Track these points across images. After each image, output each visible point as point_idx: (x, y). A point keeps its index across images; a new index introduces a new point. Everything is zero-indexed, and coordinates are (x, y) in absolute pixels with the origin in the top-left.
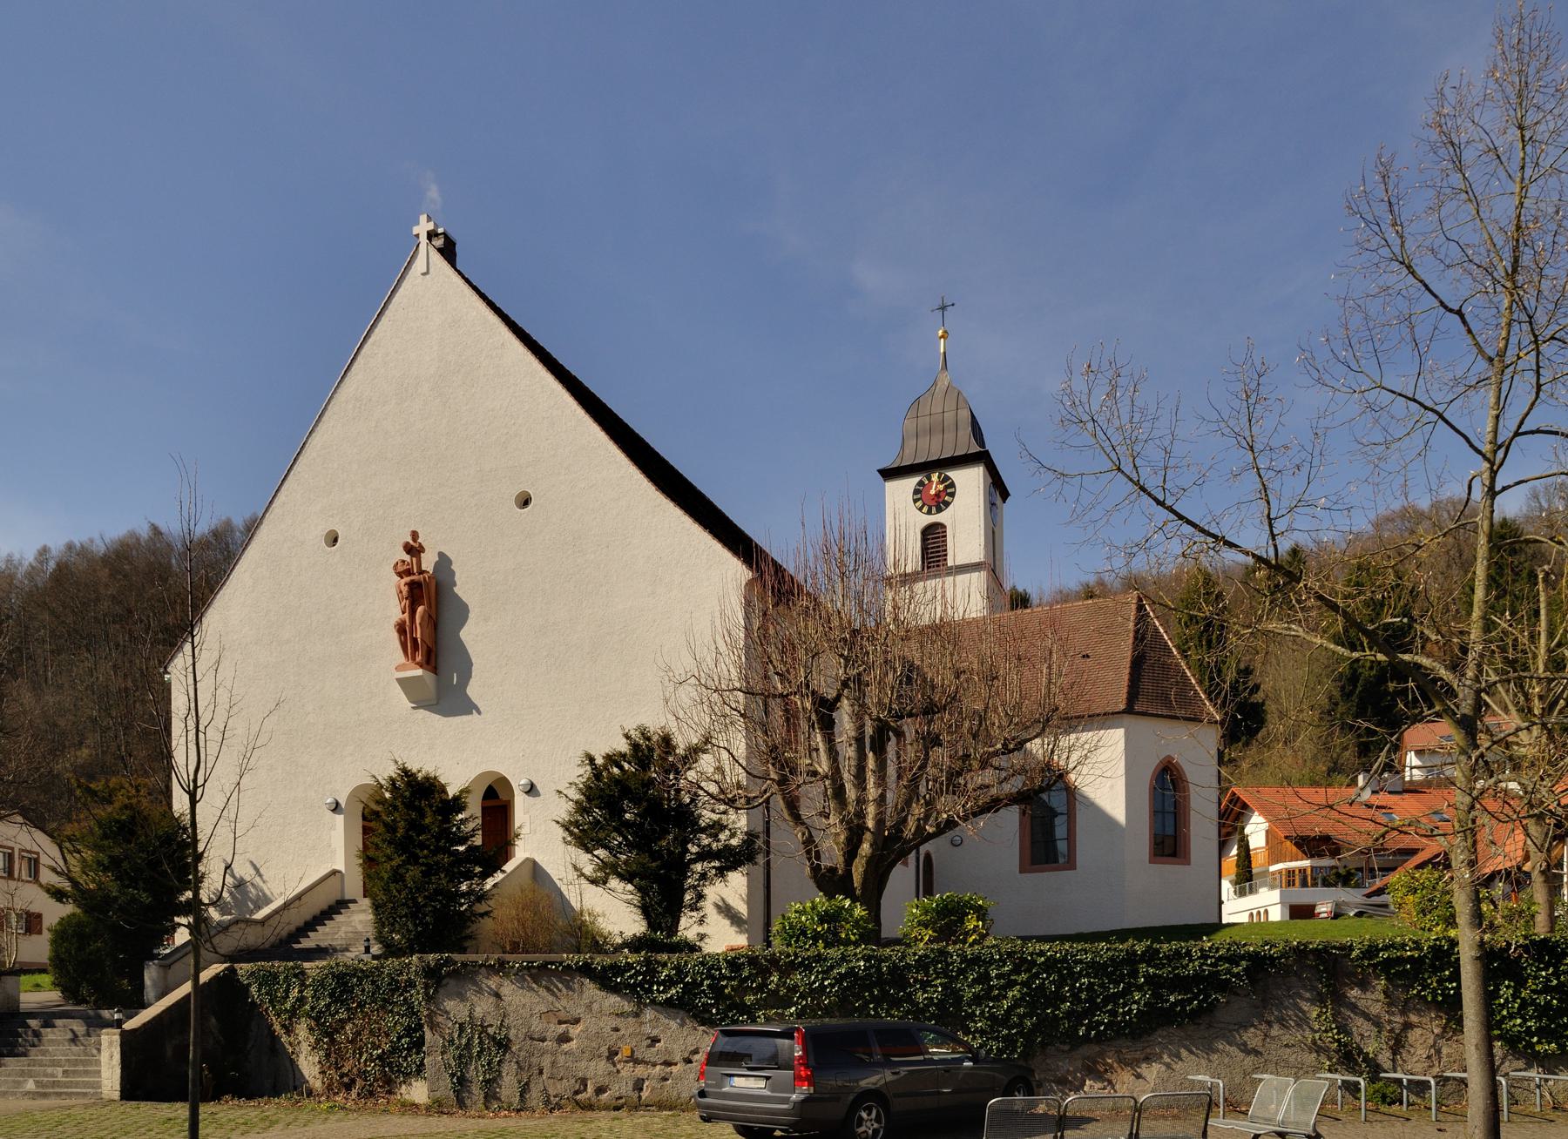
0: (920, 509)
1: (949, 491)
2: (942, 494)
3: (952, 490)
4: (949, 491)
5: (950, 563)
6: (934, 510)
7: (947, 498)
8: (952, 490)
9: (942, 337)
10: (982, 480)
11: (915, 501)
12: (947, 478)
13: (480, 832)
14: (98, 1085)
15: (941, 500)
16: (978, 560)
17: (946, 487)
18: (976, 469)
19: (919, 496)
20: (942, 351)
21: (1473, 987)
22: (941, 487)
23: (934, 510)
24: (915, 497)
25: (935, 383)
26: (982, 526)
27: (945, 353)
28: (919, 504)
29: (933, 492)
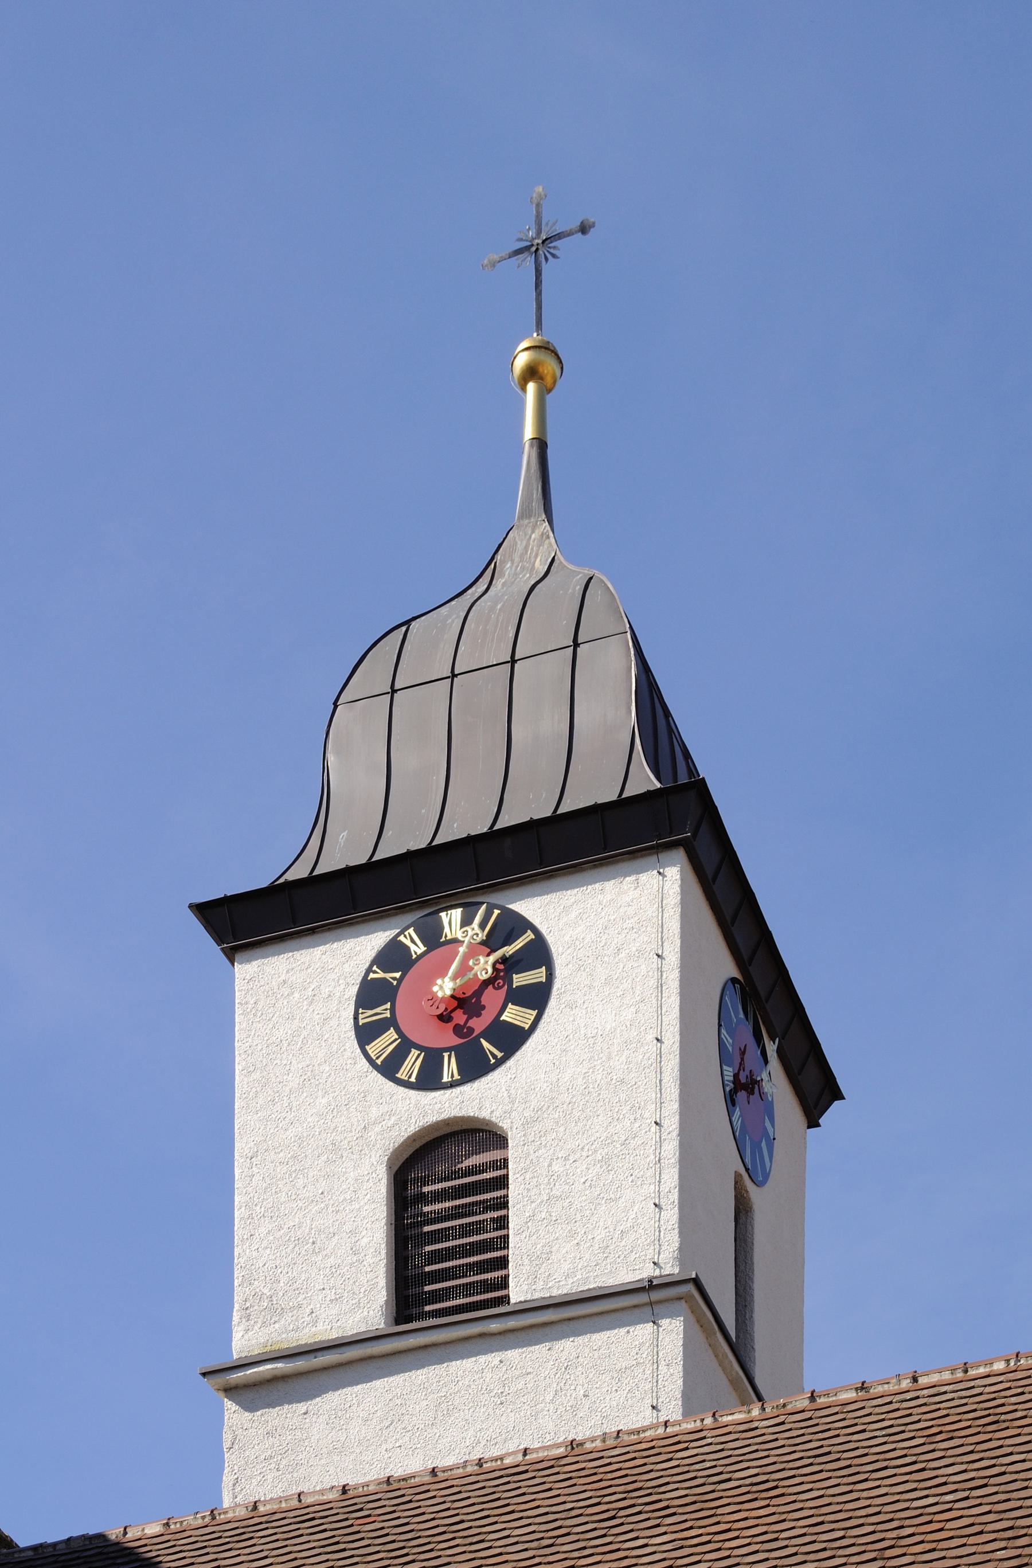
0: (389, 1068)
1: (519, 980)
2: (492, 998)
3: (538, 975)
4: (519, 980)
5: (518, 1293)
6: (450, 1068)
7: (513, 1014)
8: (538, 975)
9: (531, 372)
10: (674, 926)
11: (365, 1034)
12: (517, 924)
13: (225, 1450)
14: (426, 1305)
15: (478, 1024)
16: (646, 1272)
17: (508, 966)
18: (649, 879)
19: (383, 1011)
20: (529, 431)
21: (399, 1346)
22: (484, 966)
23: (450, 1068)
24: (367, 1017)
25: (532, 198)
26: (672, 1123)
27: (541, 444)
28: (385, 1043)
29: (445, 987)
